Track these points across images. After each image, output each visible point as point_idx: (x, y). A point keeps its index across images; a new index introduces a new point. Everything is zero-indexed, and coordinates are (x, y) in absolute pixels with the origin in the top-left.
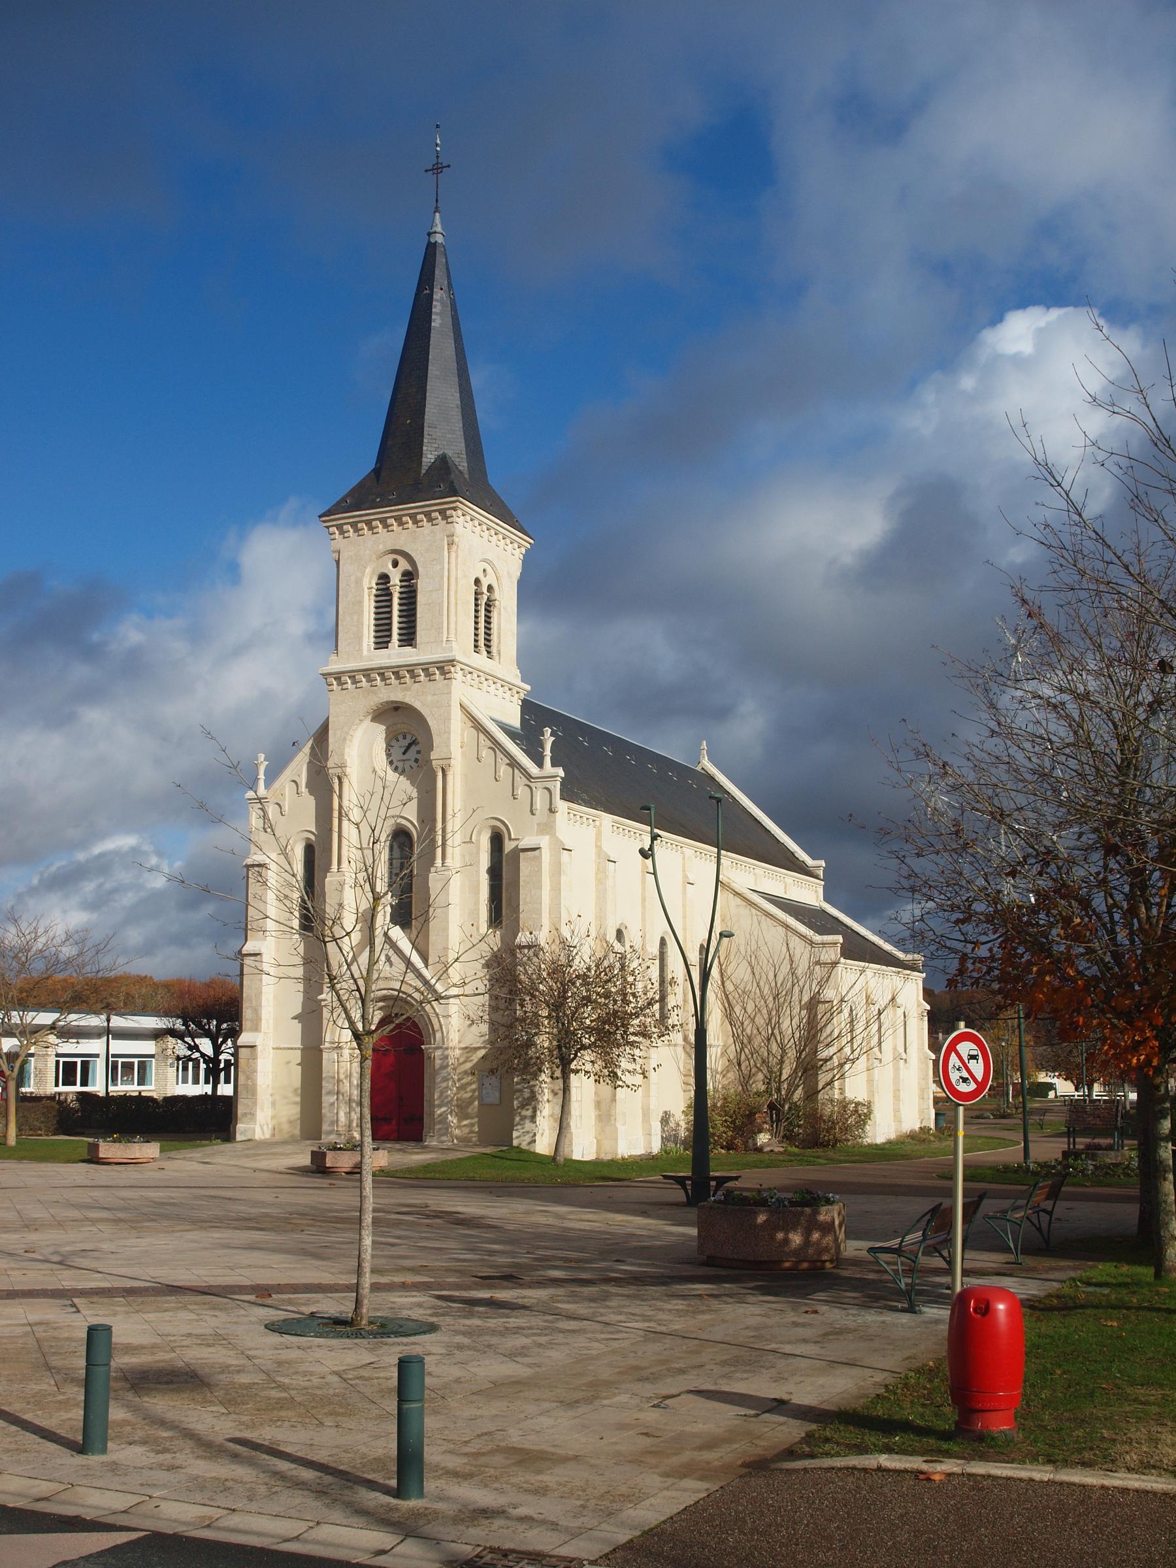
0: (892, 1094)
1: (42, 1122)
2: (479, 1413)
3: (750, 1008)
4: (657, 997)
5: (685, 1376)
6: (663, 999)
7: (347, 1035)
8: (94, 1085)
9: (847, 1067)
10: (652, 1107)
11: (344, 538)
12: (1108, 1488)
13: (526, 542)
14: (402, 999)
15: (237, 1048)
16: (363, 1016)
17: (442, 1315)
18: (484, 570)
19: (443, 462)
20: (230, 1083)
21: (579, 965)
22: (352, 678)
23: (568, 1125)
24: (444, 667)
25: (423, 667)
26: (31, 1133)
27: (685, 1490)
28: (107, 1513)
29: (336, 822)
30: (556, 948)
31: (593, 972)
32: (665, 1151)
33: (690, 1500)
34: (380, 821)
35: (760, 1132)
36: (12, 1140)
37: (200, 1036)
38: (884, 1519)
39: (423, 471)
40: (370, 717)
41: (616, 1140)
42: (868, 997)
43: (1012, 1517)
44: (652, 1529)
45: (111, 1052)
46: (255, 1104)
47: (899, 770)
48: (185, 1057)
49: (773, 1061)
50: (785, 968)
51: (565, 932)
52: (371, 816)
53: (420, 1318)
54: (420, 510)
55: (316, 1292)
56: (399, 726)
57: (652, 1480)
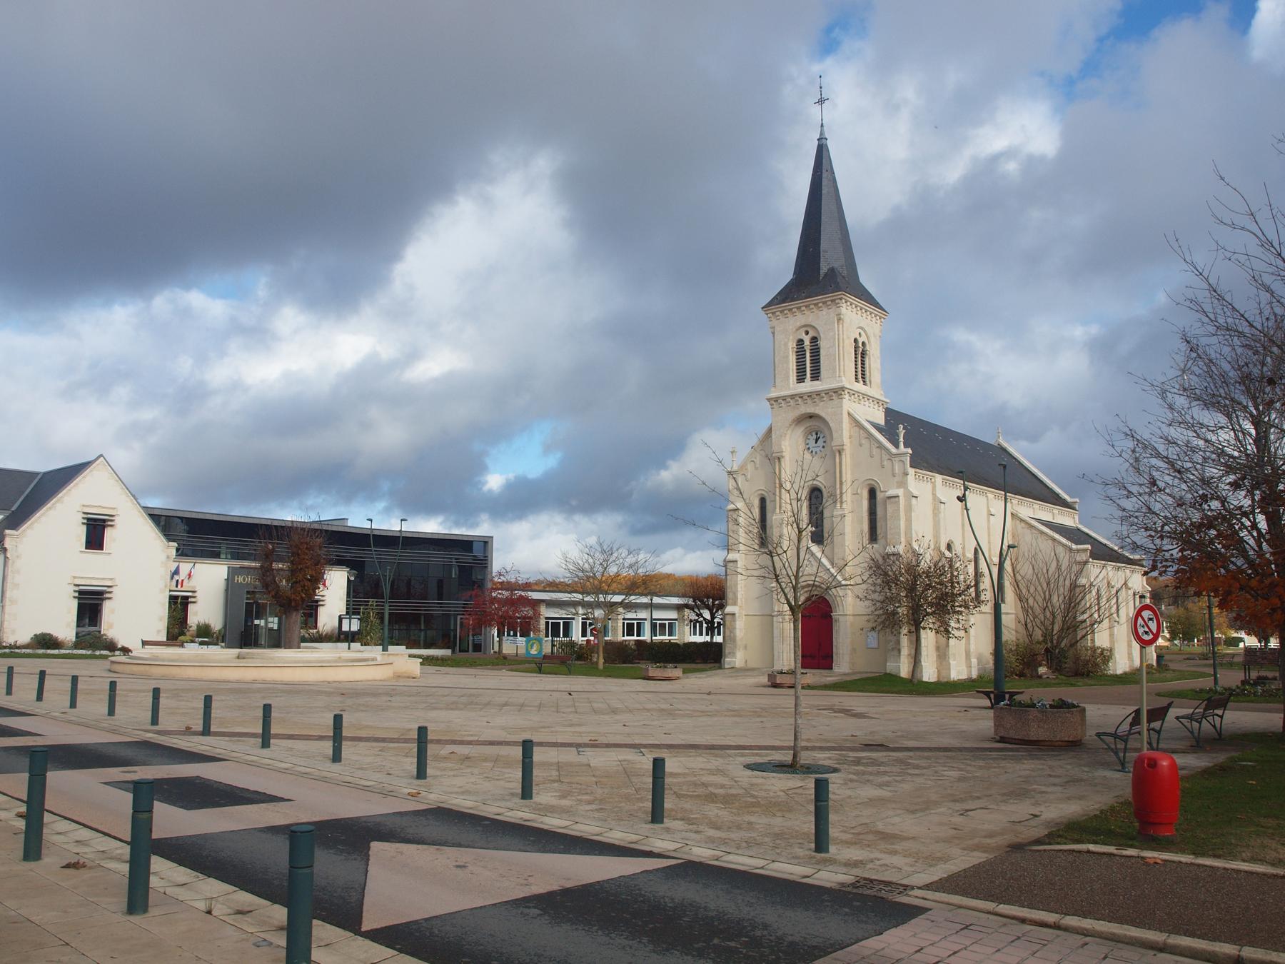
2: (860, 813)
6: (977, 585)
7: (786, 607)
9: (1096, 626)
10: (972, 650)
12: (1228, 870)
16: (794, 597)
18: (860, 334)
24: (838, 392)
27: (974, 857)
35: (1040, 665)
39: (821, 278)
42: (1109, 583)
43: (1165, 881)
46: (736, 647)
48: (695, 620)
49: (1047, 623)
50: (1054, 565)
54: (829, 299)
57: (956, 851)
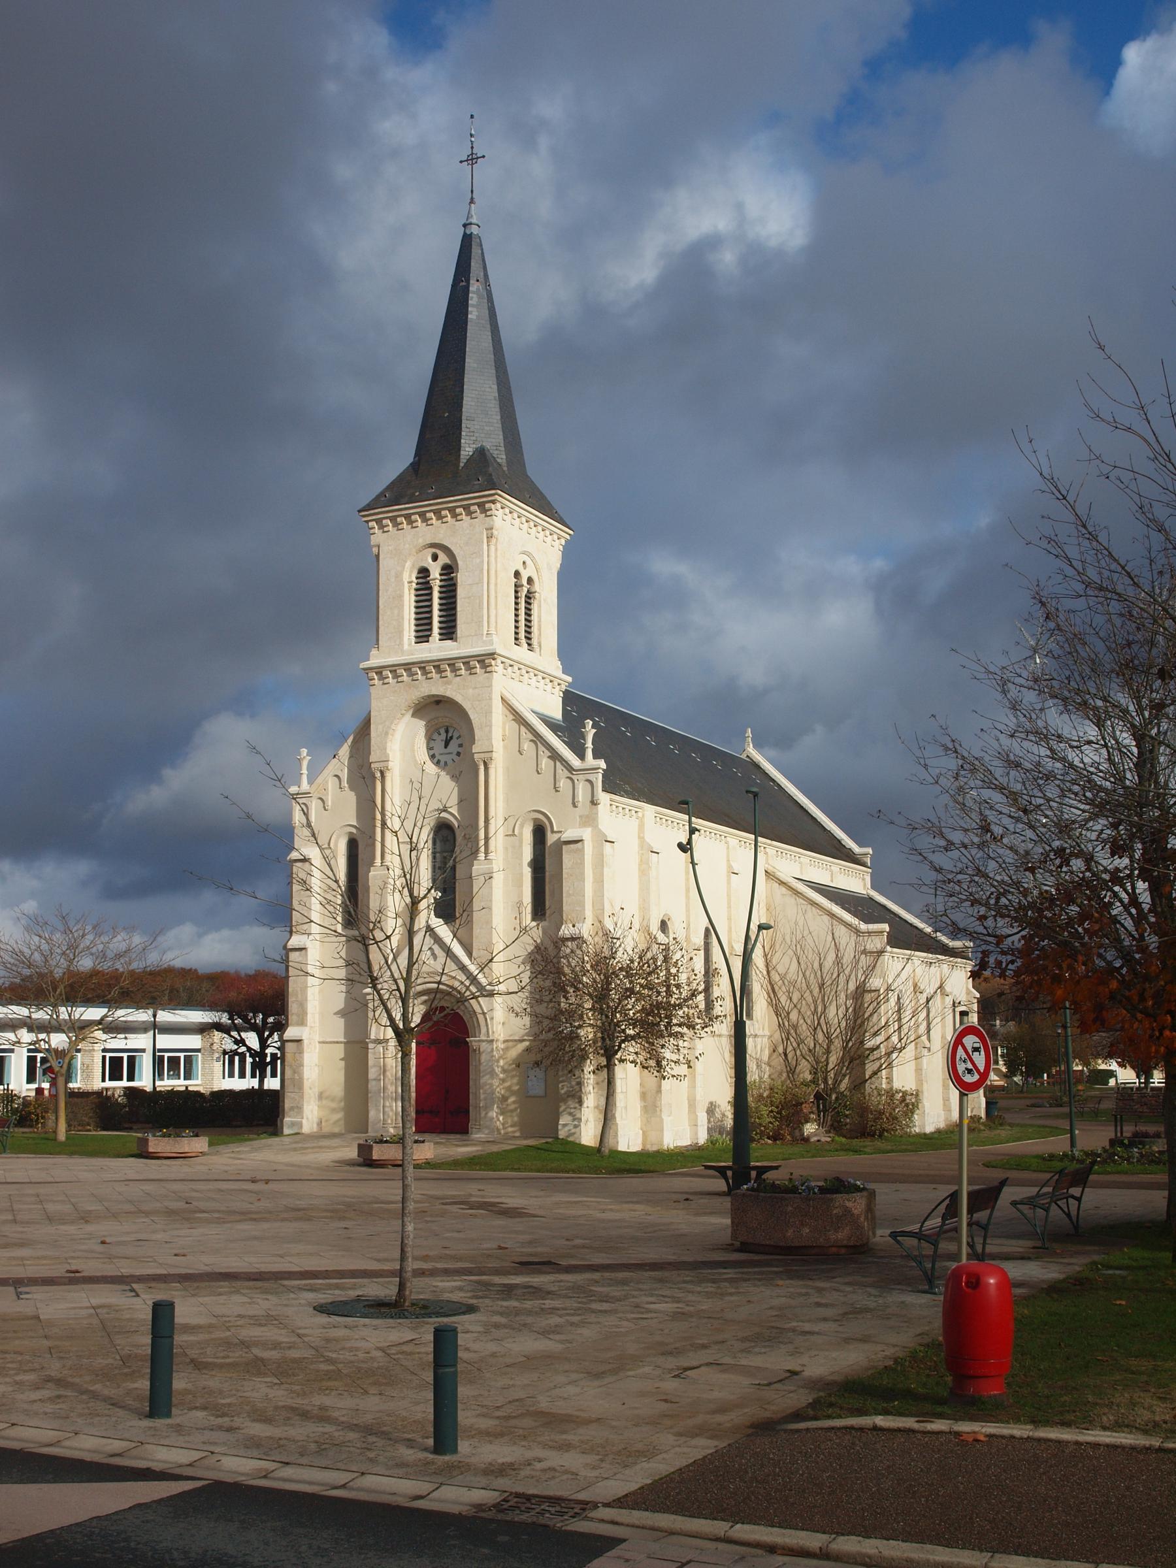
0: (941, 1083)
1: (91, 1118)
3: (796, 996)
4: (701, 987)
5: (708, 1351)
6: (707, 990)
7: (390, 1033)
8: (140, 1080)
9: (894, 1055)
10: (698, 1097)
11: (384, 532)
12: (1082, 1444)
13: (566, 534)
14: (442, 991)
15: (283, 1042)
17: (481, 1298)
18: (524, 563)
19: (481, 453)
20: (276, 1076)
21: (622, 957)
22: (393, 672)
23: (614, 1117)
24: (485, 661)
25: (464, 660)
26: (80, 1128)
28: (174, 1466)
29: (378, 830)
30: (599, 939)
31: (636, 964)
32: (712, 1141)
33: (698, 1455)
34: (417, 830)
36: (62, 1136)
37: (246, 1030)
38: (872, 1470)
39: (462, 465)
40: (411, 712)
41: (662, 1131)
42: (915, 986)
43: (988, 1468)
44: (661, 1479)
45: (158, 1047)
46: (302, 1097)
47: (926, 766)
48: (231, 1051)
50: (831, 957)
51: (609, 925)
52: (409, 825)
53: (461, 1300)
54: (459, 504)
55: (363, 1278)
56: (440, 720)
57: (666, 1439)
